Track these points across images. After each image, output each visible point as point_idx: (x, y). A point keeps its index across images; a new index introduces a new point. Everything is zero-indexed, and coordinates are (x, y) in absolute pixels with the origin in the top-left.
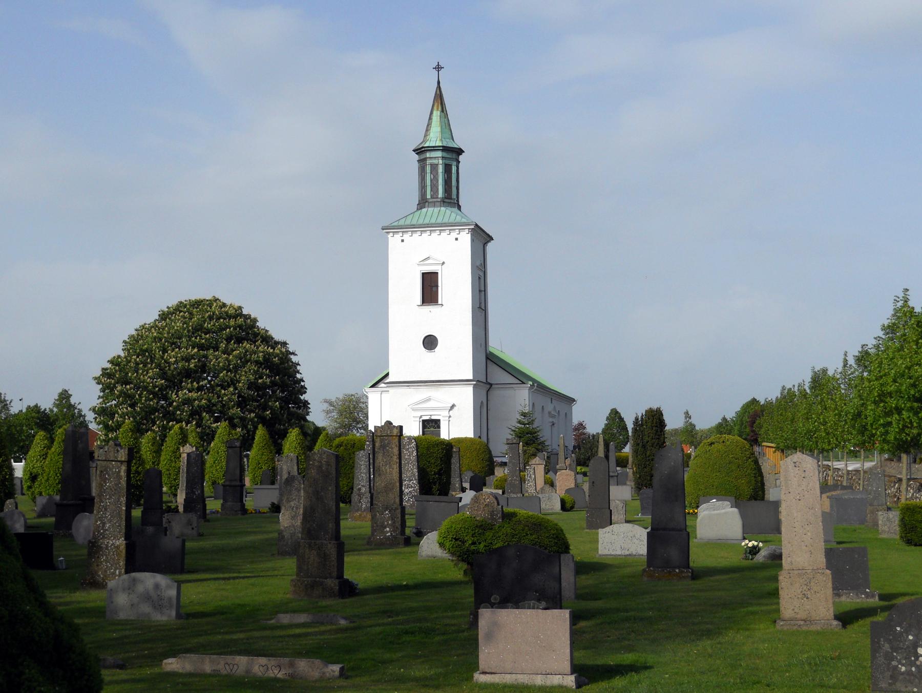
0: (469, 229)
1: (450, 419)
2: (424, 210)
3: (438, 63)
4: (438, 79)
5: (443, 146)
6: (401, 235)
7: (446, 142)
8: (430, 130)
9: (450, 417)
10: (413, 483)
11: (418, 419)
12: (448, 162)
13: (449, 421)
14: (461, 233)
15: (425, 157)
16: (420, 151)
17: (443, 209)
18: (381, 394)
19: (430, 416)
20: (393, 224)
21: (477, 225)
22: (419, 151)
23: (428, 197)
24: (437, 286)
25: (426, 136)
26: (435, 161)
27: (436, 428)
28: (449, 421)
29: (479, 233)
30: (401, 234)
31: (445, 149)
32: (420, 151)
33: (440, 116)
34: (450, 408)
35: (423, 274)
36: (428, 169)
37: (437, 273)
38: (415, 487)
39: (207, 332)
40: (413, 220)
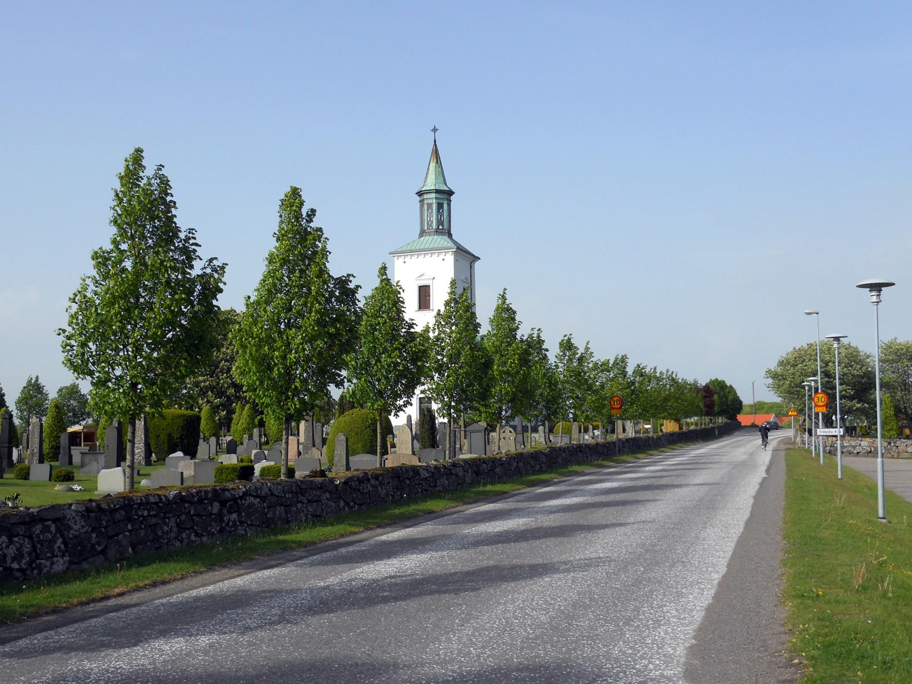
16: (420, 194)
17: (436, 237)
26: (430, 201)
30: (403, 257)
32: (420, 194)
35: (420, 287)
36: (426, 206)
37: (429, 286)
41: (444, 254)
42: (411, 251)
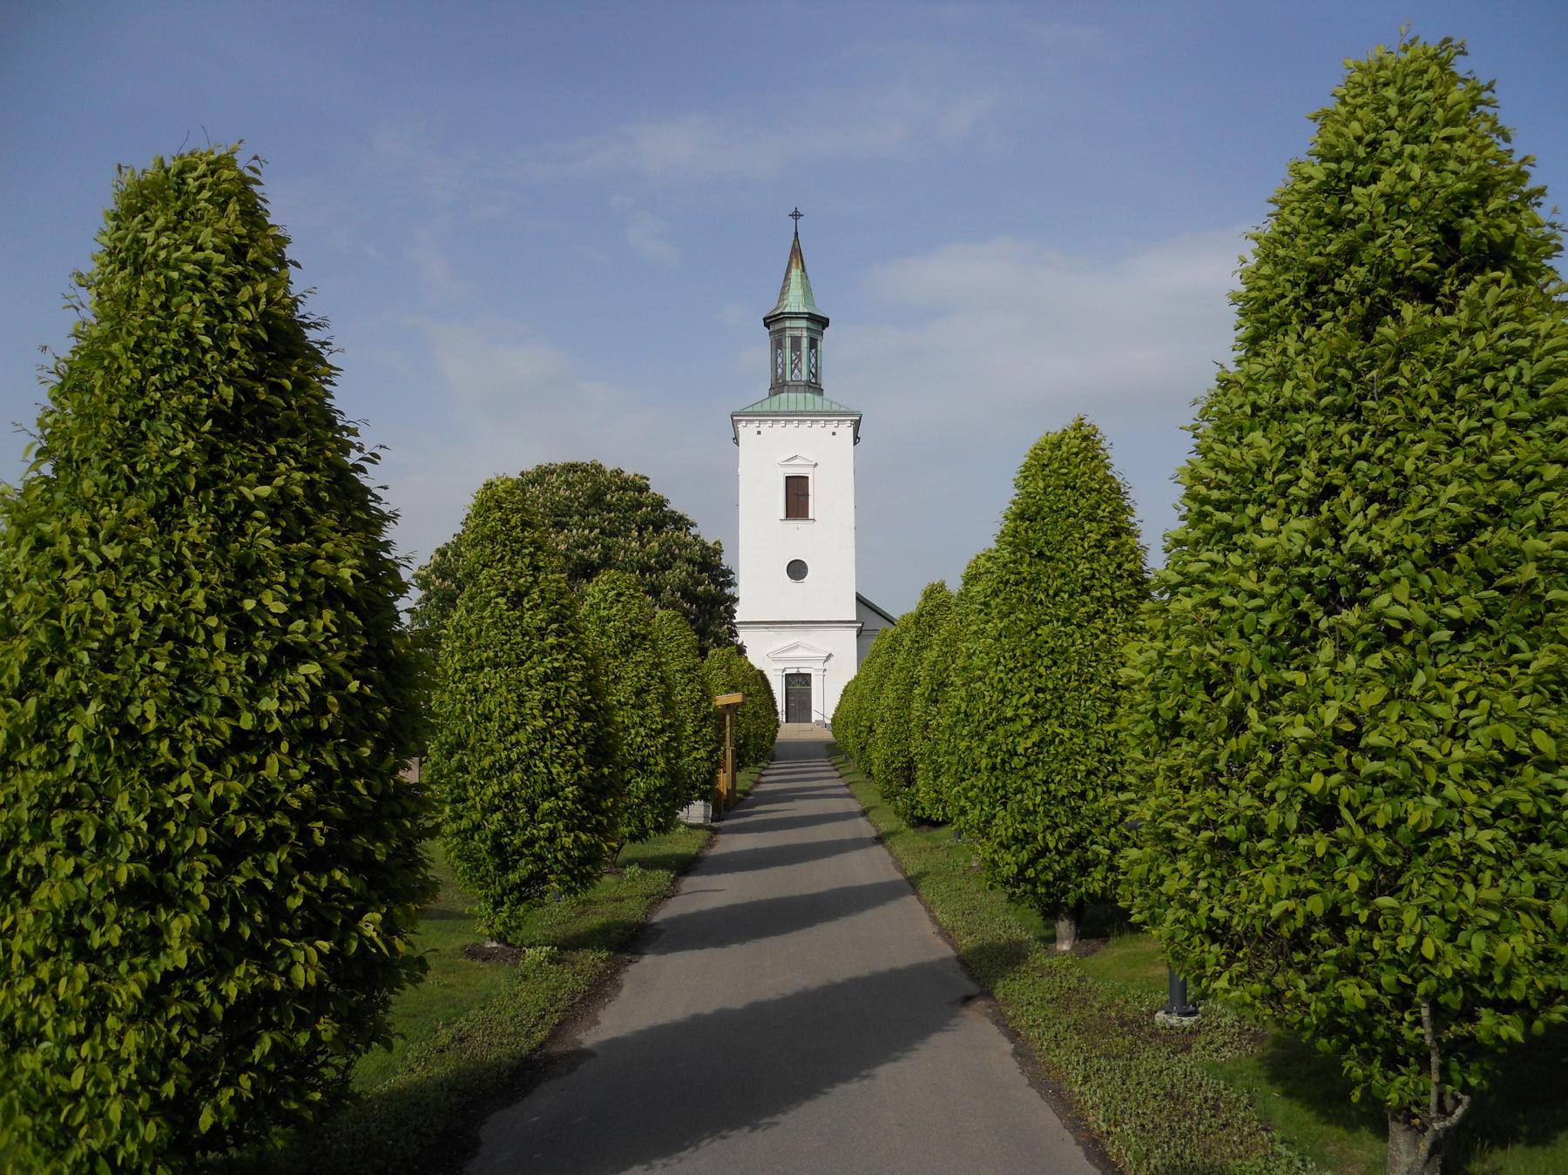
2: (784, 396)
12: (814, 336)
24: (807, 495)
26: (797, 333)
30: (757, 424)
31: (812, 318)
36: (788, 343)
39: (609, 508)
42: (776, 414)
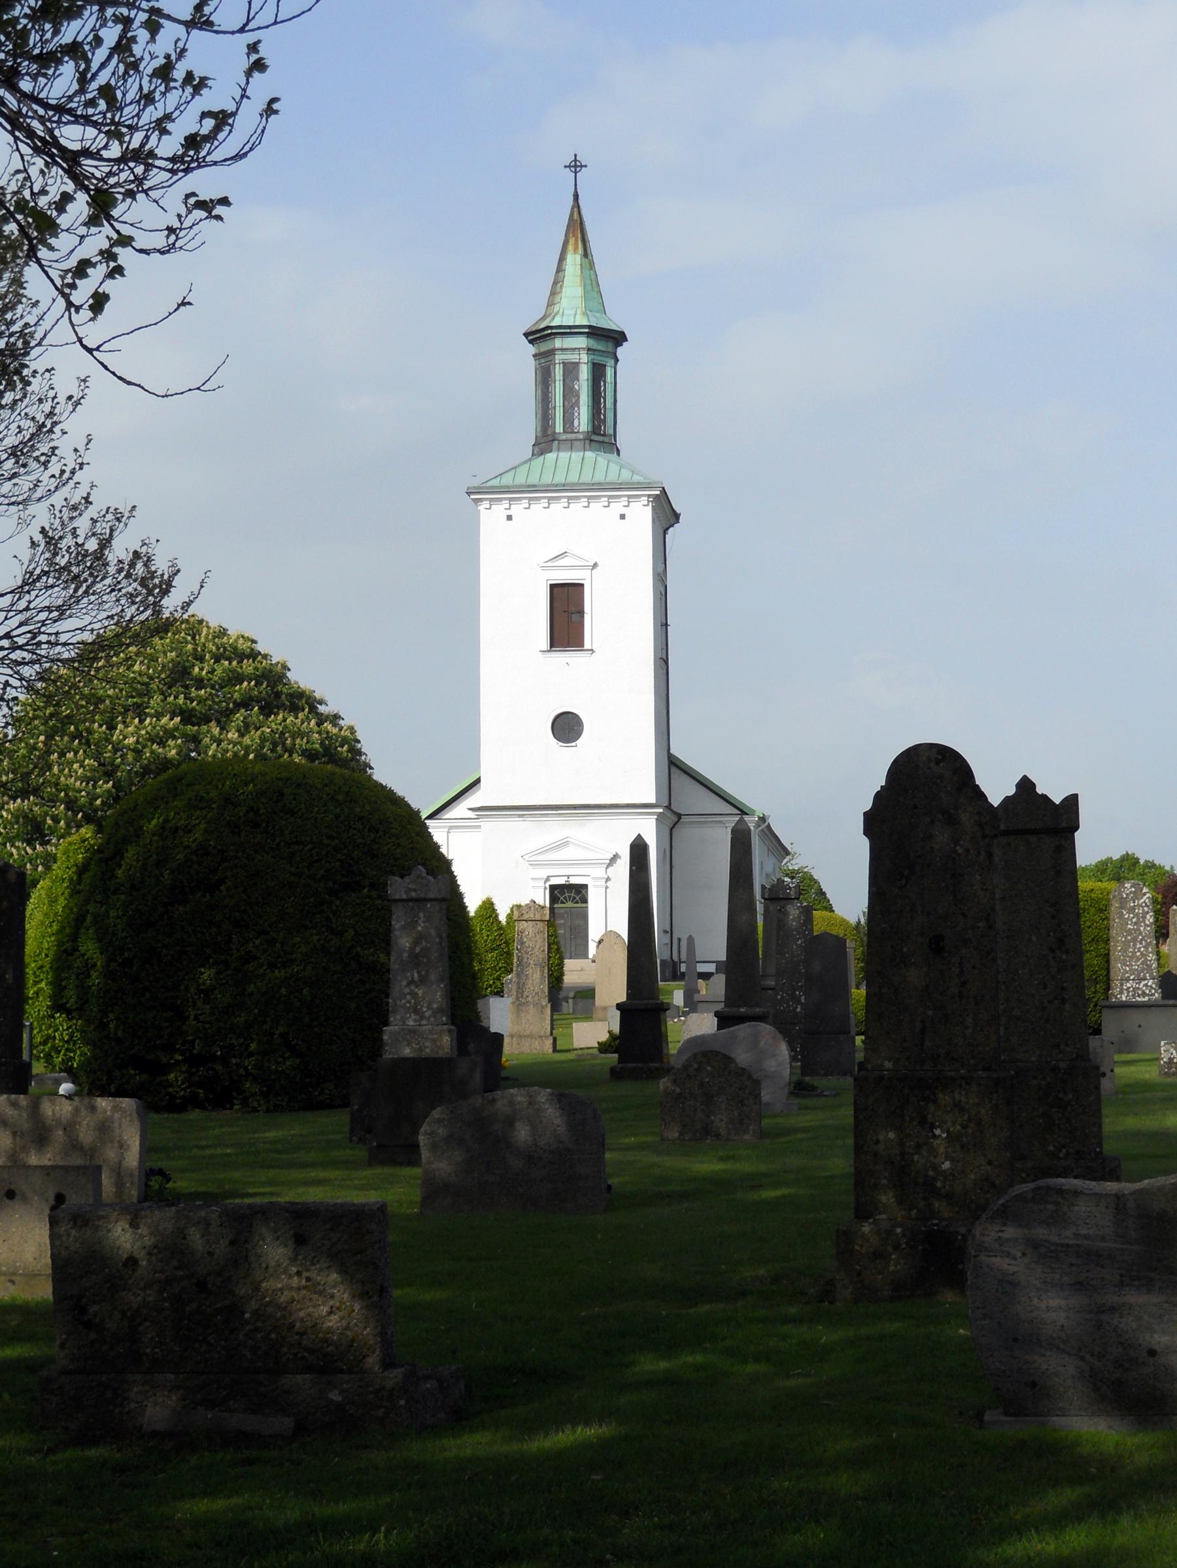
0: (649, 496)
1: (608, 884)
2: (551, 457)
3: (575, 155)
4: (576, 188)
5: (590, 327)
6: (507, 506)
7: (594, 319)
8: (561, 292)
9: (608, 879)
10: (1146, 985)
11: (542, 884)
12: (599, 359)
13: (607, 888)
14: (631, 504)
15: (552, 347)
16: (536, 336)
17: (589, 454)
18: (448, 832)
19: (566, 878)
20: (489, 484)
21: (664, 491)
22: (538, 335)
23: (557, 431)
24: (581, 612)
25: (550, 304)
26: (572, 357)
27: (577, 902)
28: (607, 888)
29: (663, 506)
31: (594, 332)
32: (536, 336)
33: (581, 265)
34: (608, 861)
35: (553, 587)
36: (558, 372)
37: (582, 585)
38: (1154, 995)
39: (200, 683)
40: (543, 476)
41: (624, 501)
